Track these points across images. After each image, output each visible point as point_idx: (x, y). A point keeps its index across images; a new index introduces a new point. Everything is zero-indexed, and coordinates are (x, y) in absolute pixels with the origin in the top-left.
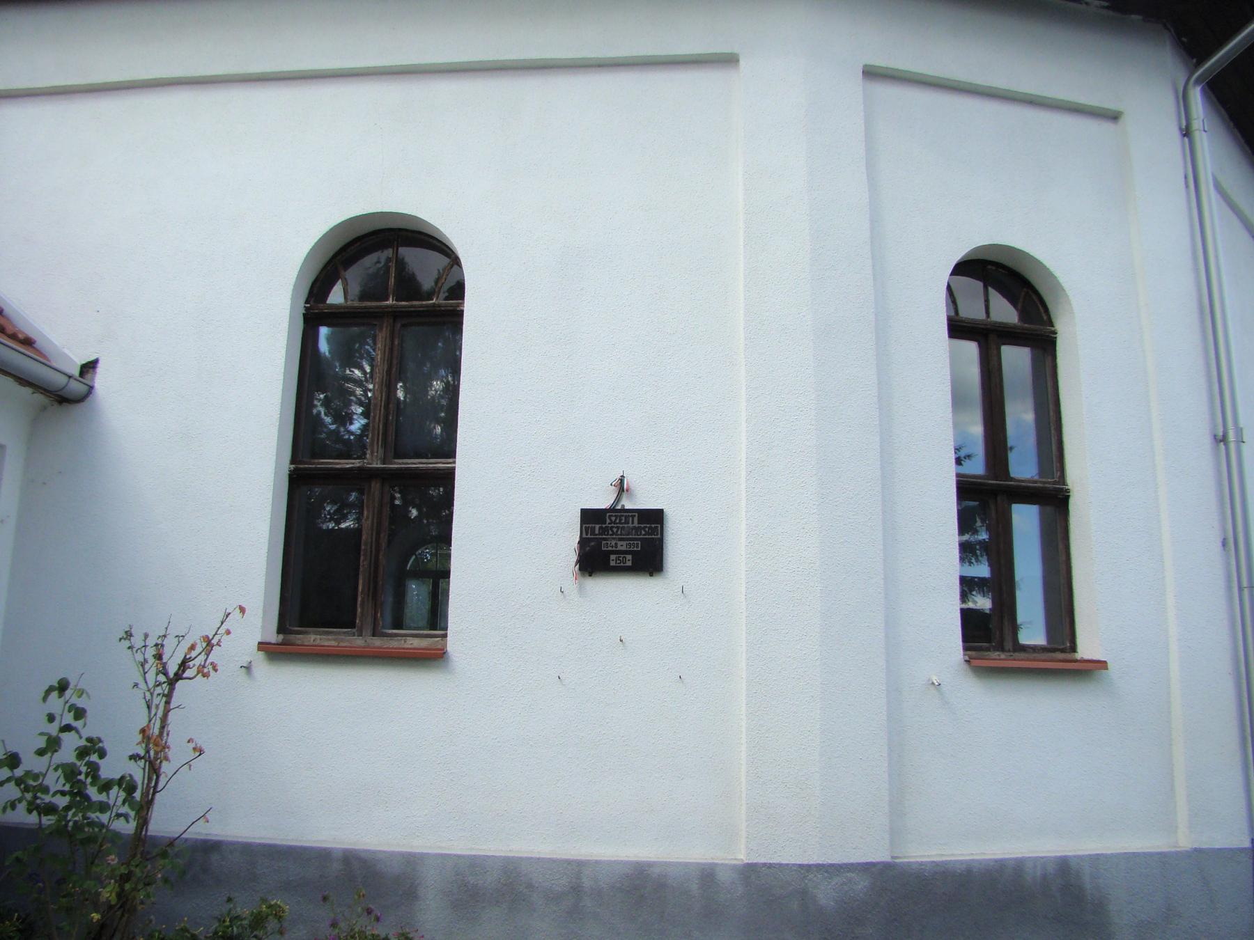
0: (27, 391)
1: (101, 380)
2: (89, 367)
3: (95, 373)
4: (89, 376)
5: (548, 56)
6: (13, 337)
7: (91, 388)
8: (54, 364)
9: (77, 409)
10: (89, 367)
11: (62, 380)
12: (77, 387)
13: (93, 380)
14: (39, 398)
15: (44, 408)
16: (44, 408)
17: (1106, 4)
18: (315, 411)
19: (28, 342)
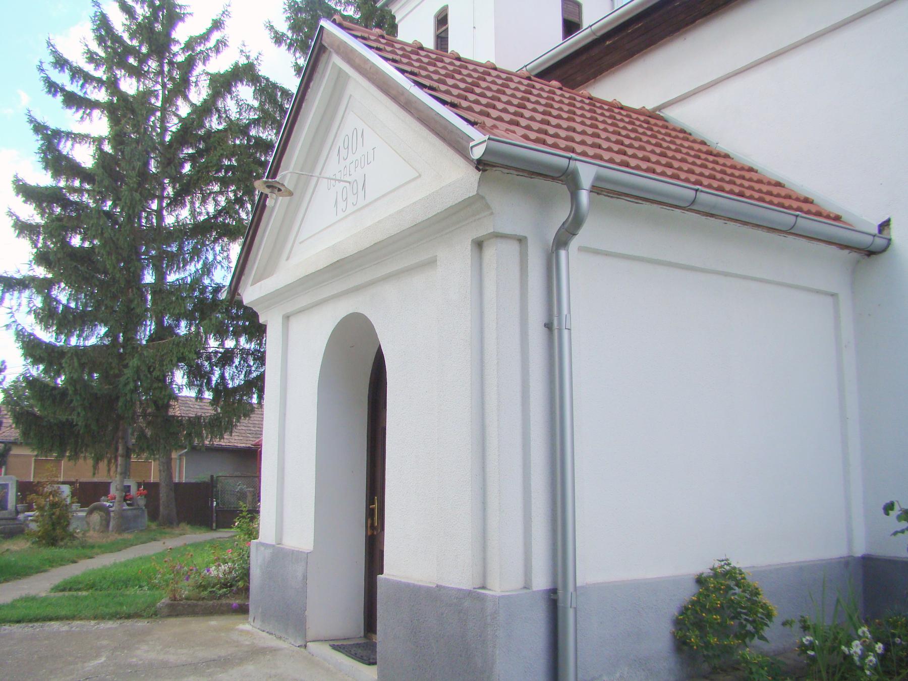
0: (846, 252)
1: (895, 232)
2: (885, 226)
3: (890, 229)
4: (885, 232)
5: (833, 23)
6: (828, 217)
7: (890, 240)
8: (857, 229)
9: (886, 254)
10: (885, 226)
11: (870, 239)
12: (880, 242)
13: (889, 234)
14: (854, 255)
15: (858, 262)
16: (858, 262)
17: (3, 470)
18: (806, 643)
19: (837, 218)
